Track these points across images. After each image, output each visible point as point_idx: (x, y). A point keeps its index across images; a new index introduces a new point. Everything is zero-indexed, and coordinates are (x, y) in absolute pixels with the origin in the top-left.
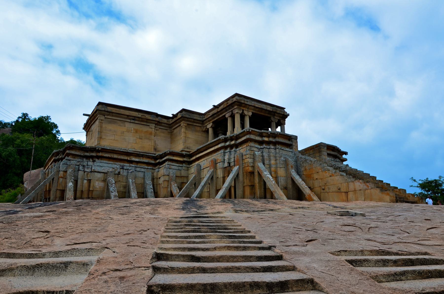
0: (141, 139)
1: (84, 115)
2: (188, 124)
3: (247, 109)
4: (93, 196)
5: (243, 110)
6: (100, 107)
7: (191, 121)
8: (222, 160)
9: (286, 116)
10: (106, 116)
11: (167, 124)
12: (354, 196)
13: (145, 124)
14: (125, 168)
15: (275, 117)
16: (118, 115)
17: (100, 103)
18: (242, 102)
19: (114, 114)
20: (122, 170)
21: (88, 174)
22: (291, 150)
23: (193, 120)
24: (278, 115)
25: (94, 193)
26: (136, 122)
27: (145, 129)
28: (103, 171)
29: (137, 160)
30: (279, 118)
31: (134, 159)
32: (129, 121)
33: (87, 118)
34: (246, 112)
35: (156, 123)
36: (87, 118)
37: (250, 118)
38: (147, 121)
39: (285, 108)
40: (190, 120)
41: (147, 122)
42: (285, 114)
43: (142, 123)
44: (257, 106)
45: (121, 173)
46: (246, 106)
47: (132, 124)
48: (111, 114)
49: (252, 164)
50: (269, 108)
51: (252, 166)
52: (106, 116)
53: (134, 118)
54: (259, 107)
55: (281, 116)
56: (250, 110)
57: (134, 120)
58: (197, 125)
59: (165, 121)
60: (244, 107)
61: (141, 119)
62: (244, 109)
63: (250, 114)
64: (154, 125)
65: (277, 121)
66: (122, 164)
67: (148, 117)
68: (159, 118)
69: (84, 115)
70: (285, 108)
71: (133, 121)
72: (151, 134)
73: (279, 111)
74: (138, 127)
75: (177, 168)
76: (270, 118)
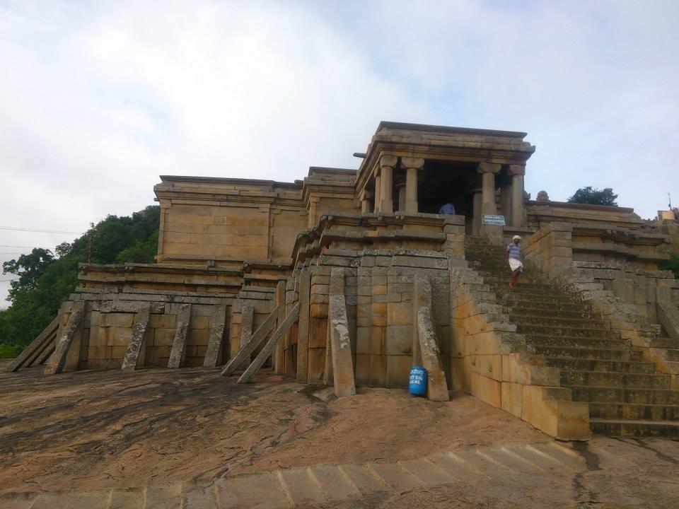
0: (243, 235)
1: (356, 155)
2: (321, 198)
3: (410, 155)
4: (113, 357)
5: (399, 159)
6: (384, 132)
7: (327, 192)
8: (347, 278)
9: (528, 152)
10: (173, 201)
11: (295, 200)
12: (23, 419)
13: (251, 205)
14: (177, 299)
15: (494, 161)
16: (194, 196)
17: (384, 125)
18: (394, 139)
19: (187, 195)
20: (167, 305)
21: (105, 317)
22: (440, 255)
23: (331, 189)
24: (507, 154)
25: (115, 351)
26: (232, 204)
27: (251, 215)
28: (132, 310)
29: (203, 282)
30: (504, 162)
31: (197, 280)
32: (218, 203)
33: (361, 160)
34: (407, 162)
35: (272, 200)
36: (361, 160)
37: (419, 172)
38: (253, 199)
39: (524, 135)
40: (325, 188)
41: (253, 202)
42: (522, 149)
43: (245, 205)
44: (434, 142)
45: (167, 311)
46: (405, 147)
47: (224, 209)
48: (181, 195)
49: (321, 300)
50: (473, 142)
51: (323, 303)
52: (173, 201)
53: (228, 198)
54: (442, 143)
55: (510, 154)
56: (418, 155)
57: (226, 201)
58: (344, 196)
59: (292, 194)
60: (402, 150)
61: (239, 198)
62: (403, 154)
63: (420, 163)
64: (269, 205)
65: (498, 169)
66: (172, 292)
67: (253, 191)
68: (278, 190)
69: (356, 155)
70: (524, 135)
71: (226, 203)
72: (262, 224)
73: (505, 144)
74: (238, 214)
75: (262, 296)
76: (477, 164)
